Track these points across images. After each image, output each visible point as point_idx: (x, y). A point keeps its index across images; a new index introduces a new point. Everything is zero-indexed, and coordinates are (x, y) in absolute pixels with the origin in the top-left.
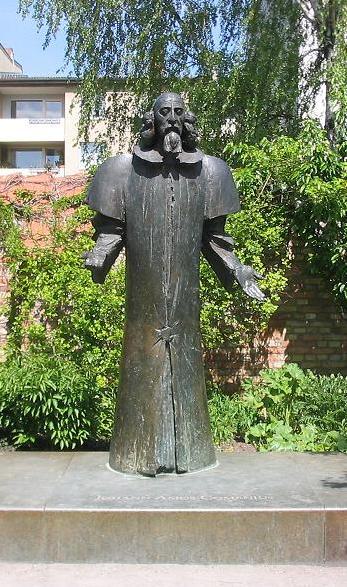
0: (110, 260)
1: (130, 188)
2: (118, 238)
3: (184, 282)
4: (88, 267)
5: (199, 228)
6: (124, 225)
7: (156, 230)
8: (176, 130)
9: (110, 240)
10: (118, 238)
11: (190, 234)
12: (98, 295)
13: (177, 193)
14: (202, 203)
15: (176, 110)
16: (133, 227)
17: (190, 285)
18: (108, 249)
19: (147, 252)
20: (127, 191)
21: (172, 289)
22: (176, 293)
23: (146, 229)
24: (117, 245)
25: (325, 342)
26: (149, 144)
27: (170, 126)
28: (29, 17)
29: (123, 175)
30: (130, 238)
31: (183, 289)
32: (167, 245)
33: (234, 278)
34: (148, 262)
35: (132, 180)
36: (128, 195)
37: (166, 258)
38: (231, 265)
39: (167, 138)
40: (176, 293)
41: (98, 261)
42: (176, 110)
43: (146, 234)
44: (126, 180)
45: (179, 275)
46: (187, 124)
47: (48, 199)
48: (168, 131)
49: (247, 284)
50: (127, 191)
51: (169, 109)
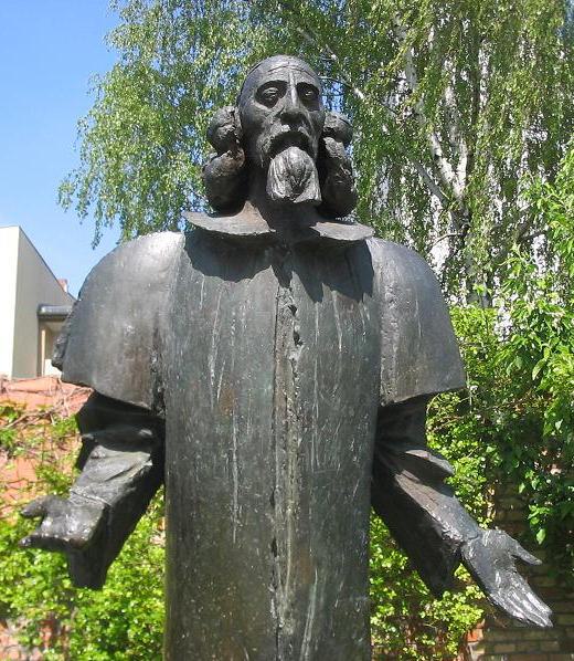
0: (117, 523)
1: (173, 319)
2: (141, 460)
3: (331, 584)
4: (50, 544)
5: (366, 426)
6: (152, 419)
7: (249, 429)
8: (305, 146)
9: (120, 466)
10: (141, 460)
11: (345, 443)
12: (125, 601)
13: (309, 324)
14: (375, 356)
15: (301, 88)
16: (181, 426)
17: (346, 593)
18: (112, 491)
19: (224, 498)
20: (165, 325)
21: (300, 600)
22: (311, 616)
23: (218, 430)
24: (138, 481)
25: (543, 648)
26: (231, 192)
27: (286, 128)
28: (73, 207)
29: (154, 287)
30: (172, 460)
31: (329, 601)
32: (287, 480)
33: (459, 558)
34: (225, 526)
35: (182, 295)
36: (168, 339)
37: (284, 513)
38: (453, 531)
39: (278, 165)
40: (311, 616)
41: (79, 526)
42: (301, 88)
43: (218, 443)
44: (164, 299)
45: (319, 565)
46: (329, 140)
47: (48, 417)
48: (280, 144)
49: (498, 578)
50: (165, 325)
51: (282, 87)
